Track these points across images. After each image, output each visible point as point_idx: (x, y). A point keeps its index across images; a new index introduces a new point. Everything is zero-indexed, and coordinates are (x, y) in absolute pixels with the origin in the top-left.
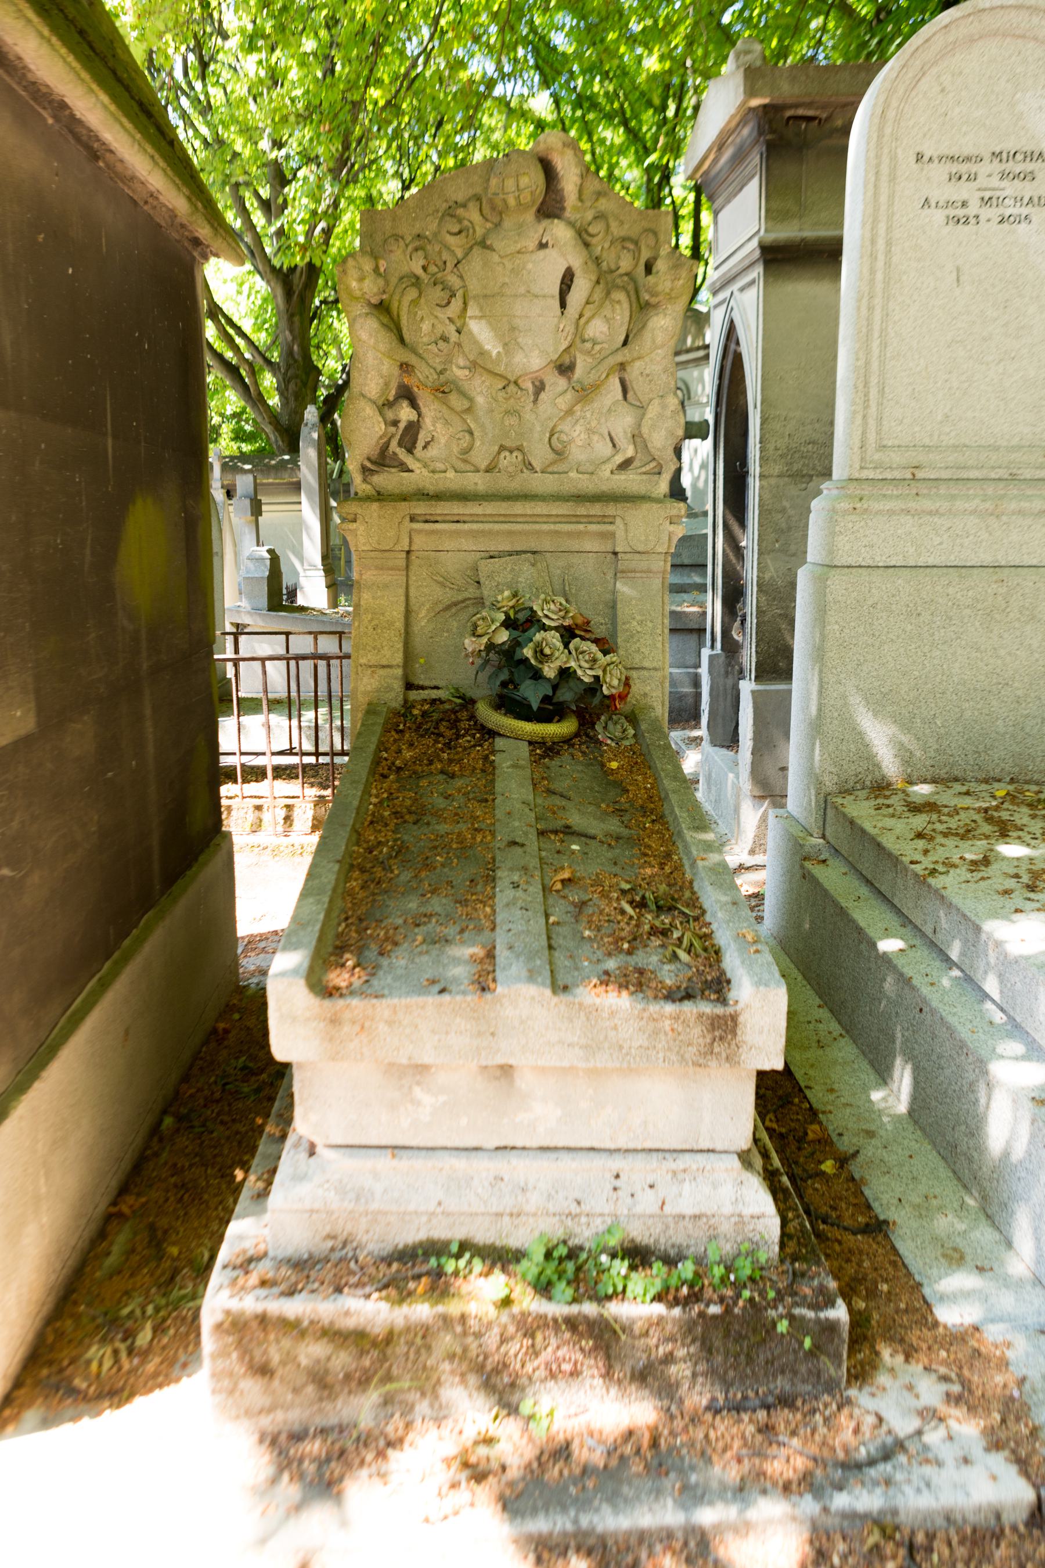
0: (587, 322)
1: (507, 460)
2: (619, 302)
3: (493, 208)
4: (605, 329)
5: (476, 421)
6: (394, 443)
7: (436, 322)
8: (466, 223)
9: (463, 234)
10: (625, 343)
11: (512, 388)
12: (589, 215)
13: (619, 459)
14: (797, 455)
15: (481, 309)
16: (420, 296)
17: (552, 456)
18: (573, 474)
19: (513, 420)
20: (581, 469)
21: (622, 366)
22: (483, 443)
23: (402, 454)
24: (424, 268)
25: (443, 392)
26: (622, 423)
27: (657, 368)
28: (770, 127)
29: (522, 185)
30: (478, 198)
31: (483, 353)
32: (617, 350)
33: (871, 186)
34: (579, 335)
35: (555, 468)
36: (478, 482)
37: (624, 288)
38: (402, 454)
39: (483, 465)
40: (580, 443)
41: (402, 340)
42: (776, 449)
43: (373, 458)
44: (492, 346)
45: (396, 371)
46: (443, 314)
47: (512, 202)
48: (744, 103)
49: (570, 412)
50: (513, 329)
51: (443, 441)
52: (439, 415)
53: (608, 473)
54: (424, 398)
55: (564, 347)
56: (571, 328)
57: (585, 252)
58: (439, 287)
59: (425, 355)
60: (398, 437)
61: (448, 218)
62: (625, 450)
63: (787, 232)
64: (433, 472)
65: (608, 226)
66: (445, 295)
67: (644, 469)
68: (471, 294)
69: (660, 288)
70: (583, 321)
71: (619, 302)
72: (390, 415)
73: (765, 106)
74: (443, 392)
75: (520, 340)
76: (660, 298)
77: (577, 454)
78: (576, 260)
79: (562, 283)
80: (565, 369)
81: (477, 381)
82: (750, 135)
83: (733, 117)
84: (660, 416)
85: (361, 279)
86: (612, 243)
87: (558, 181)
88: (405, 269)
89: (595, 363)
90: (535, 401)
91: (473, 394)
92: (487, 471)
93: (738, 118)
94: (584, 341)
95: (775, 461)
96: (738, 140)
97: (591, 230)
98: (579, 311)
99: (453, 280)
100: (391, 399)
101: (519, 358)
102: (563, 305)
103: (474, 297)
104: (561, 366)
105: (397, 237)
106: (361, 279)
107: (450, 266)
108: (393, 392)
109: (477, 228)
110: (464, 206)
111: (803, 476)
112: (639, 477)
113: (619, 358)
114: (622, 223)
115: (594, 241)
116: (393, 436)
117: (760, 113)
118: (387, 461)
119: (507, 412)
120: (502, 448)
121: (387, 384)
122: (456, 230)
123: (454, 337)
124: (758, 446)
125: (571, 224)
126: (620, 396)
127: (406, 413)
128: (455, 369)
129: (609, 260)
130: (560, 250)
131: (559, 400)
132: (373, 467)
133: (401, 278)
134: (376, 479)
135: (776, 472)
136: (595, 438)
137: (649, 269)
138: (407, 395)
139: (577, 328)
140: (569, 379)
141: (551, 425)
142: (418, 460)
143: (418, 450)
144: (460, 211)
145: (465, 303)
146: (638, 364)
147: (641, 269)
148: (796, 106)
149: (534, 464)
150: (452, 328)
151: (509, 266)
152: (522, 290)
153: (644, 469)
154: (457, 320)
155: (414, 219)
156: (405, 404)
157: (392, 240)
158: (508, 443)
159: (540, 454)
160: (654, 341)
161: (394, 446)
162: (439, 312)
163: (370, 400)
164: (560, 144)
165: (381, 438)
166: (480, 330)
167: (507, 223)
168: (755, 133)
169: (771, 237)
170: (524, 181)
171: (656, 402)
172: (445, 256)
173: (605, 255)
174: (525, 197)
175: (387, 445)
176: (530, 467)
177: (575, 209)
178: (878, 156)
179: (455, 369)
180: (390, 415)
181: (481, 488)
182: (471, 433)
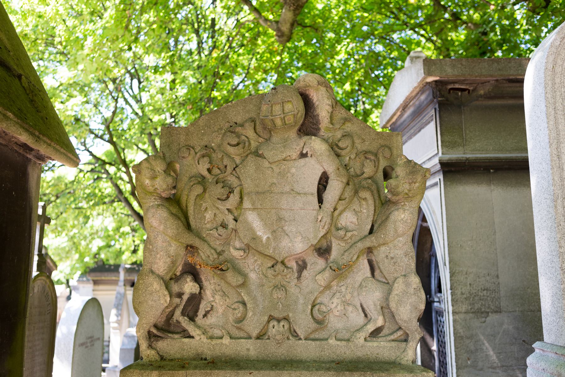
0: (340, 214)
1: (275, 329)
2: (365, 199)
3: (265, 128)
4: (355, 220)
5: (249, 294)
6: (178, 313)
7: (217, 212)
8: (243, 138)
9: (241, 146)
10: (371, 232)
11: (279, 267)
12: (339, 134)
13: (371, 328)
14: (476, 298)
15: (253, 204)
16: (205, 191)
17: (314, 325)
18: (332, 341)
19: (279, 294)
20: (340, 336)
21: (370, 250)
22: (254, 314)
23: (185, 322)
24: (209, 170)
25: (222, 270)
26: (373, 297)
27: (399, 253)
28: (440, 93)
29: (286, 110)
30: (253, 121)
31: (255, 238)
32: (365, 237)
33: (552, 118)
34: (334, 226)
35: (316, 336)
36: (249, 348)
37: (369, 189)
38: (185, 322)
39: (254, 334)
40: (337, 314)
41: (188, 227)
42: (462, 294)
43: (160, 325)
44: (263, 234)
45: (182, 252)
46: (223, 207)
47: (279, 122)
48: (424, 78)
49: (328, 287)
50: (280, 219)
51: (221, 311)
52: (218, 288)
53: (362, 341)
54: (206, 275)
55: (322, 234)
56: (327, 220)
57: (337, 161)
58: (221, 185)
59: (208, 239)
60: (181, 307)
61: (229, 134)
62: (376, 320)
63: (456, 155)
64: (211, 338)
65: (353, 143)
66: (225, 191)
67: (392, 337)
68: (245, 191)
69: (400, 189)
70: (337, 213)
71: (365, 199)
72: (175, 288)
73: (436, 81)
74: (222, 270)
75: (286, 228)
76: (401, 197)
77: (335, 322)
78: (330, 167)
79: (319, 184)
80: (323, 251)
81: (251, 260)
82: (426, 99)
83: (415, 88)
84: (405, 293)
85: (153, 178)
86: (357, 154)
87: (315, 109)
88: (194, 171)
89: (347, 247)
90: (299, 277)
91: (247, 271)
92: (258, 338)
93: (418, 90)
94: (338, 229)
95: (462, 302)
96: (417, 103)
97: (340, 144)
98: (333, 205)
99: (232, 180)
100: (178, 274)
101: (285, 243)
102: (320, 201)
103: (249, 193)
104: (320, 249)
105: (189, 147)
106: (153, 178)
107: (229, 169)
108: (180, 268)
109: (252, 142)
110: (242, 125)
111: (482, 313)
112: (389, 345)
113: (368, 243)
114: (364, 141)
115: (343, 153)
116: (177, 306)
117: (434, 86)
118: (172, 328)
119: (276, 287)
120: (271, 318)
121: (173, 263)
122: (234, 142)
123: (231, 224)
124: (449, 292)
125: (325, 140)
126: (369, 274)
127: (189, 287)
128: (232, 250)
129: (355, 167)
130: (317, 158)
131: (319, 277)
132: (158, 334)
133: (191, 178)
134: (161, 345)
135: (464, 310)
136: (350, 309)
137: (387, 176)
138: (192, 272)
139: (332, 220)
140: (327, 259)
141: (313, 298)
142: (199, 327)
143: (199, 319)
144: (238, 129)
145: (241, 198)
146: (383, 248)
147: (380, 175)
148: (454, 82)
149: (299, 333)
150: (230, 218)
151: (277, 170)
152: (287, 189)
153: (392, 337)
154: (235, 211)
155: (203, 134)
156: (189, 279)
157: (184, 149)
158: (276, 314)
159: (303, 324)
160: (396, 231)
161: (178, 315)
162: (220, 205)
163: (158, 276)
164: (316, 82)
165: (167, 307)
166: (253, 219)
167: (275, 138)
168: (431, 97)
169: (447, 157)
170: (288, 107)
171: (400, 280)
172: (226, 161)
173: (352, 163)
174: (290, 119)
175: (172, 314)
176: (295, 335)
177: (328, 129)
178: (554, 97)
179: (232, 250)
180: (175, 288)
181: (253, 353)
182: (244, 304)
